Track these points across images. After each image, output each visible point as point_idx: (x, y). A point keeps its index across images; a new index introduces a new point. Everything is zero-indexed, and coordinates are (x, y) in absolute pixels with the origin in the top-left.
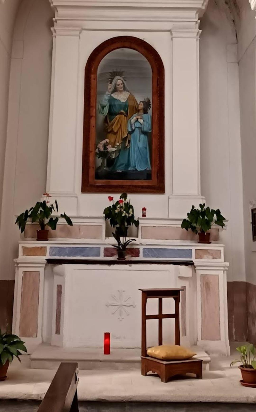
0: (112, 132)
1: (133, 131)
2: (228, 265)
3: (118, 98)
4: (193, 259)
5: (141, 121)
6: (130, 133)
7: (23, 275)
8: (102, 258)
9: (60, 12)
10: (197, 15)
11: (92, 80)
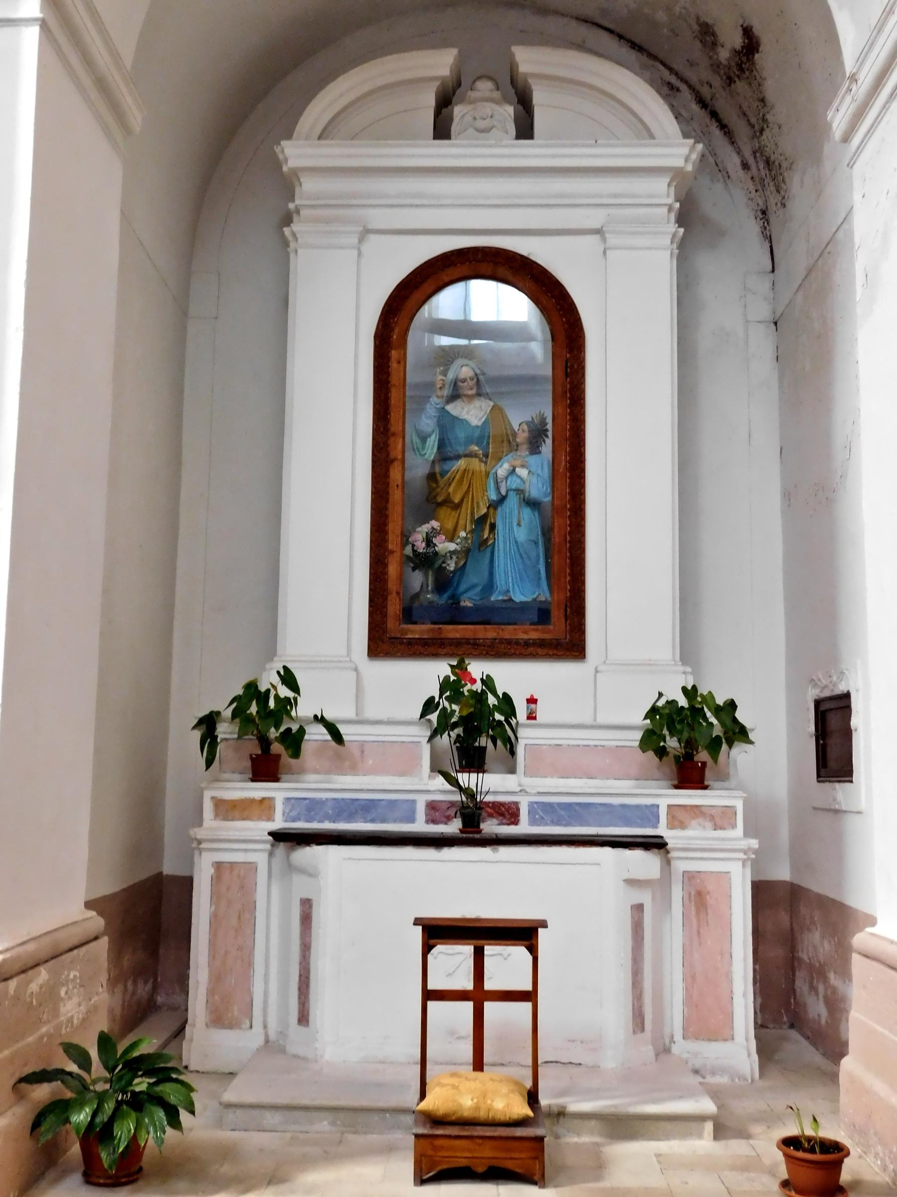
0: (447, 502)
1: (502, 499)
2: (757, 846)
3: (464, 415)
4: (662, 830)
5: (523, 472)
6: (494, 505)
7: (213, 871)
8: (420, 826)
9: (309, 186)
10: (672, 189)
11: (394, 365)
